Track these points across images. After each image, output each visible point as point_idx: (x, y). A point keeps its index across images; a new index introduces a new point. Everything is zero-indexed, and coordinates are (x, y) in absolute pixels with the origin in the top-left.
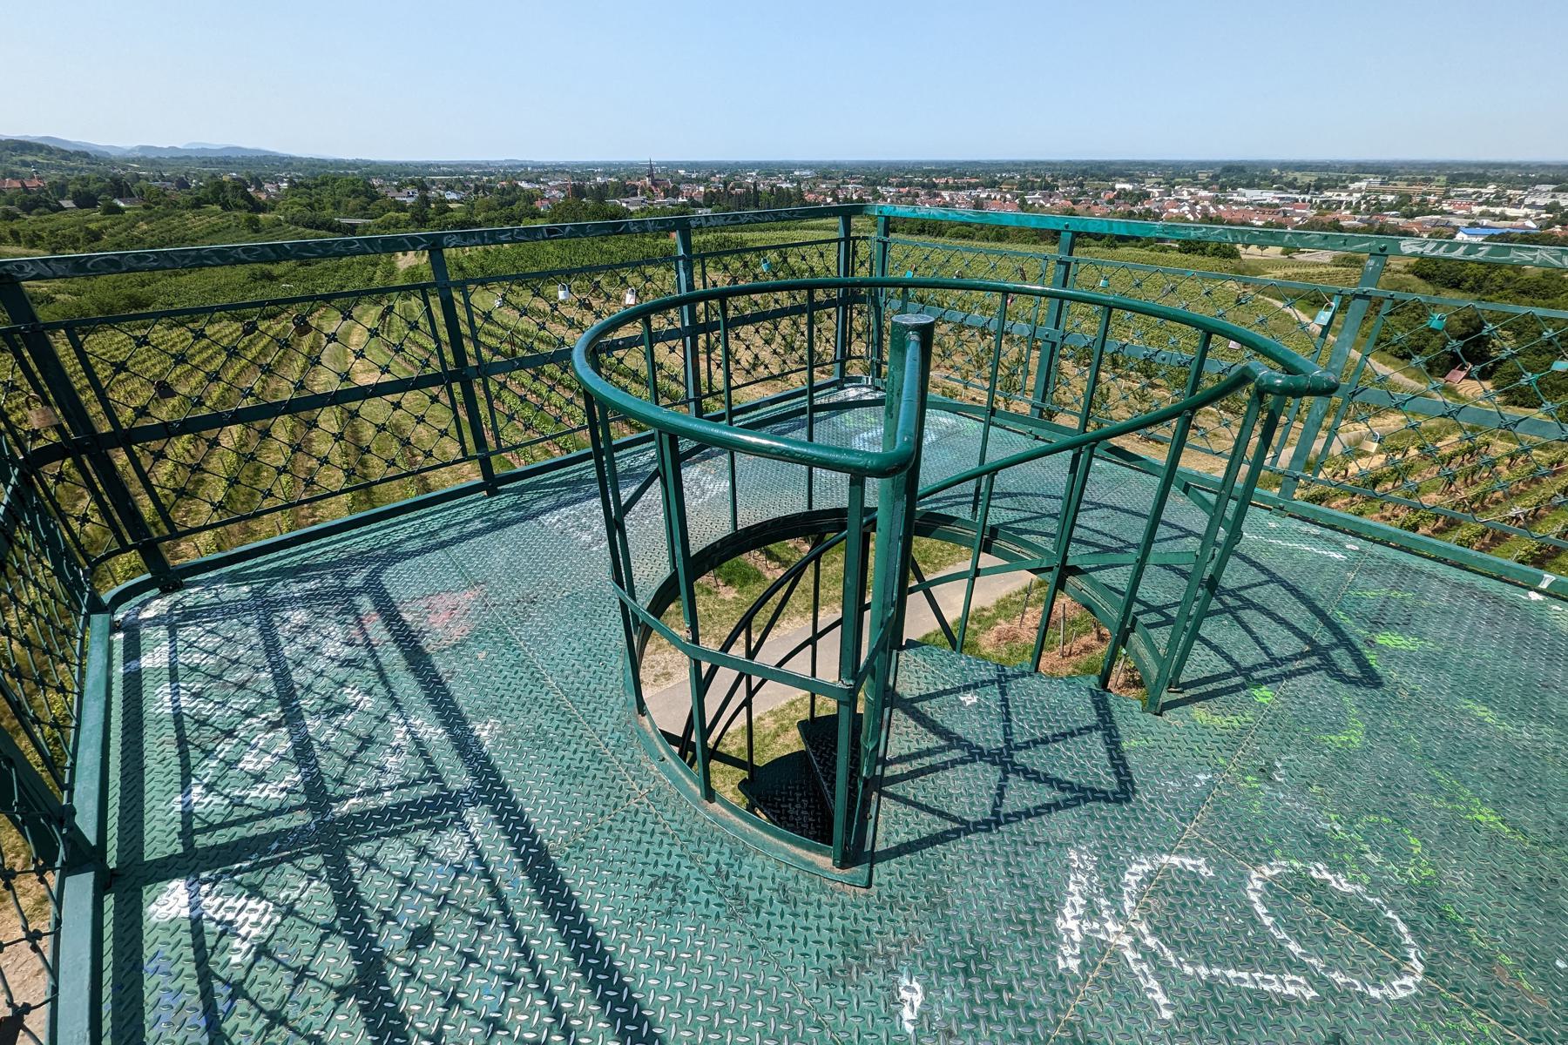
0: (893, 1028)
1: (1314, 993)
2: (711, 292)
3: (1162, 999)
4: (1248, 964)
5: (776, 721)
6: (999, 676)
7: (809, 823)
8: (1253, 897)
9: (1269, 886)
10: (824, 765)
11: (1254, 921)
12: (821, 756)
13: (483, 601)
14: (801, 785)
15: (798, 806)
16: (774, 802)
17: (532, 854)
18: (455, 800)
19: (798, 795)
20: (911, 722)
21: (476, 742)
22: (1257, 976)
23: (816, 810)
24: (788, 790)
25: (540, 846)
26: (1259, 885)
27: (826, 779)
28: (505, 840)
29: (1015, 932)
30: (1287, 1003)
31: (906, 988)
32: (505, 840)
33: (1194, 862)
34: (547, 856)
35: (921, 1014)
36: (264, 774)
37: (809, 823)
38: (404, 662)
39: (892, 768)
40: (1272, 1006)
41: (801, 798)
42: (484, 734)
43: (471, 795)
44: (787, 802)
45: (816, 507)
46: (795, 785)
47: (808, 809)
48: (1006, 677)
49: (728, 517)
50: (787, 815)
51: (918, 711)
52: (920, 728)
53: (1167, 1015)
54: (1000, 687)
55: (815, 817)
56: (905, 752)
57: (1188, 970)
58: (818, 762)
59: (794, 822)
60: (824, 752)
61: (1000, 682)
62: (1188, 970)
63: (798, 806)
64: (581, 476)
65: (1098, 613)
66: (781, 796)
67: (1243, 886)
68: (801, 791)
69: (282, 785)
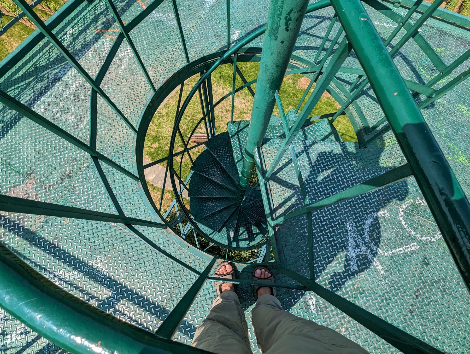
0: (309, 314)
1: (419, 247)
2: (53, 42)
3: (380, 267)
4: (401, 245)
5: (174, 100)
6: (305, 147)
7: (218, 174)
8: (401, 219)
9: (405, 213)
10: (219, 157)
11: (402, 228)
12: (217, 154)
13: (41, 186)
14: (211, 162)
15: (213, 169)
16: (205, 171)
17: (158, 311)
18: (108, 303)
19: (211, 165)
20: (278, 186)
21: (98, 271)
22: (404, 247)
23: (219, 169)
24: (207, 165)
25: (159, 307)
26: (402, 213)
27: (221, 162)
28: (143, 311)
29: (336, 264)
30: (412, 253)
31: (310, 299)
32: (143, 311)
33: (383, 213)
34: (164, 309)
35: (316, 305)
36: (5, 331)
37: (218, 174)
38: (25, 242)
39: (278, 211)
40: (408, 256)
41: (213, 166)
42: (99, 265)
43: (114, 298)
44: (209, 169)
45: (191, 61)
46: (209, 162)
47: (217, 169)
48: (308, 147)
49: (148, 86)
50: (211, 174)
51: (279, 179)
52: (283, 187)
53: (382, 272)
54: (306, 153)
55: (220, 171)
56: (280, 202)
57: (386, 254)
58: (217, 157)
59: (214, 175)
60: (217, 152)
61: (306, 151)
62: (386, 254)
63: (213, 169)
64: (35, 64)
65: (332, 93)
66: (206, 168)
67: (398, 215)
68: (212, 164)
69: (19, 332)
